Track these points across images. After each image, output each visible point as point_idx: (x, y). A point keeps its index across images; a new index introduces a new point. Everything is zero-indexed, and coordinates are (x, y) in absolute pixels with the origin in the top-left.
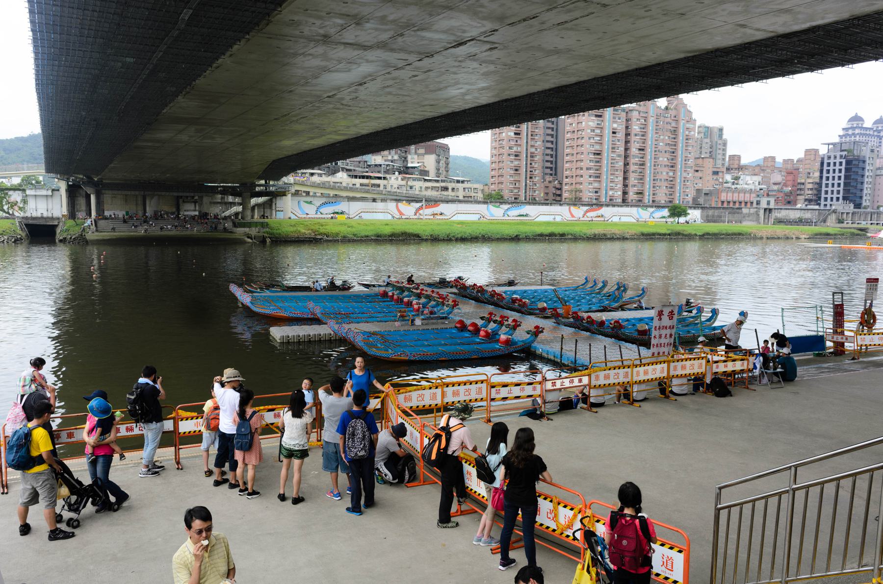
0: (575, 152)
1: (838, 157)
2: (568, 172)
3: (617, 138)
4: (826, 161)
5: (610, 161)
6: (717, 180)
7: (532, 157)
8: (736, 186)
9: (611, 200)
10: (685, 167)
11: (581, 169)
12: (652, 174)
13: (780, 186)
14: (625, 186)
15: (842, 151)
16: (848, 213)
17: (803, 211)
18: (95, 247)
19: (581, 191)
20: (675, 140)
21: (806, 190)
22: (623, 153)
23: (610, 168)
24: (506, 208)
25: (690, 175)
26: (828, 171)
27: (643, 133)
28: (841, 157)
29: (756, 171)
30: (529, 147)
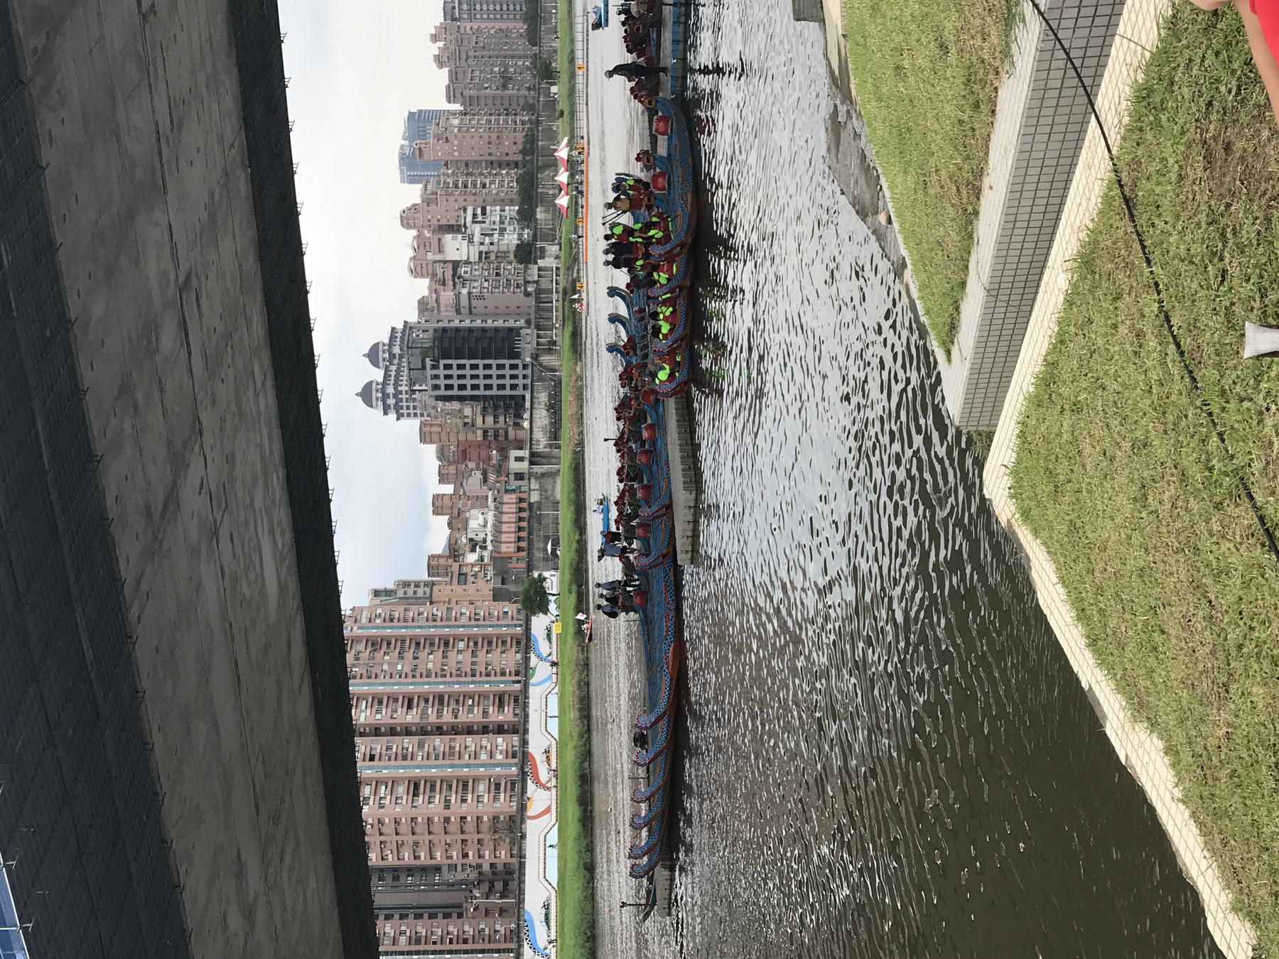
0: (411, 839)
1: (435, 372)
2: (454, 854)
3: (384, 752)
4: (442, 392)
5: (432, 762)
6: (475, 576)
7: (418, 941)
8: (489, 543)
9: (514, 756)
10: (449, 619)
11: (447, 820)
12: (460, 679)
13: (490, 470)
14: (485, 730)
15: (424, 368)
16: (538, 336)
17: (535, 405)
18: (539, 176)
19: (495, 818)
20: (393, 642)
21: (498, 426)
22: (416, 739)
23: (446, 762)
24: (531, 952)
25: (464, 610)
26: (462, 387)
27: (376, 702)
28: (434, 367)
29: (460, 525)
30: (395, 948)
